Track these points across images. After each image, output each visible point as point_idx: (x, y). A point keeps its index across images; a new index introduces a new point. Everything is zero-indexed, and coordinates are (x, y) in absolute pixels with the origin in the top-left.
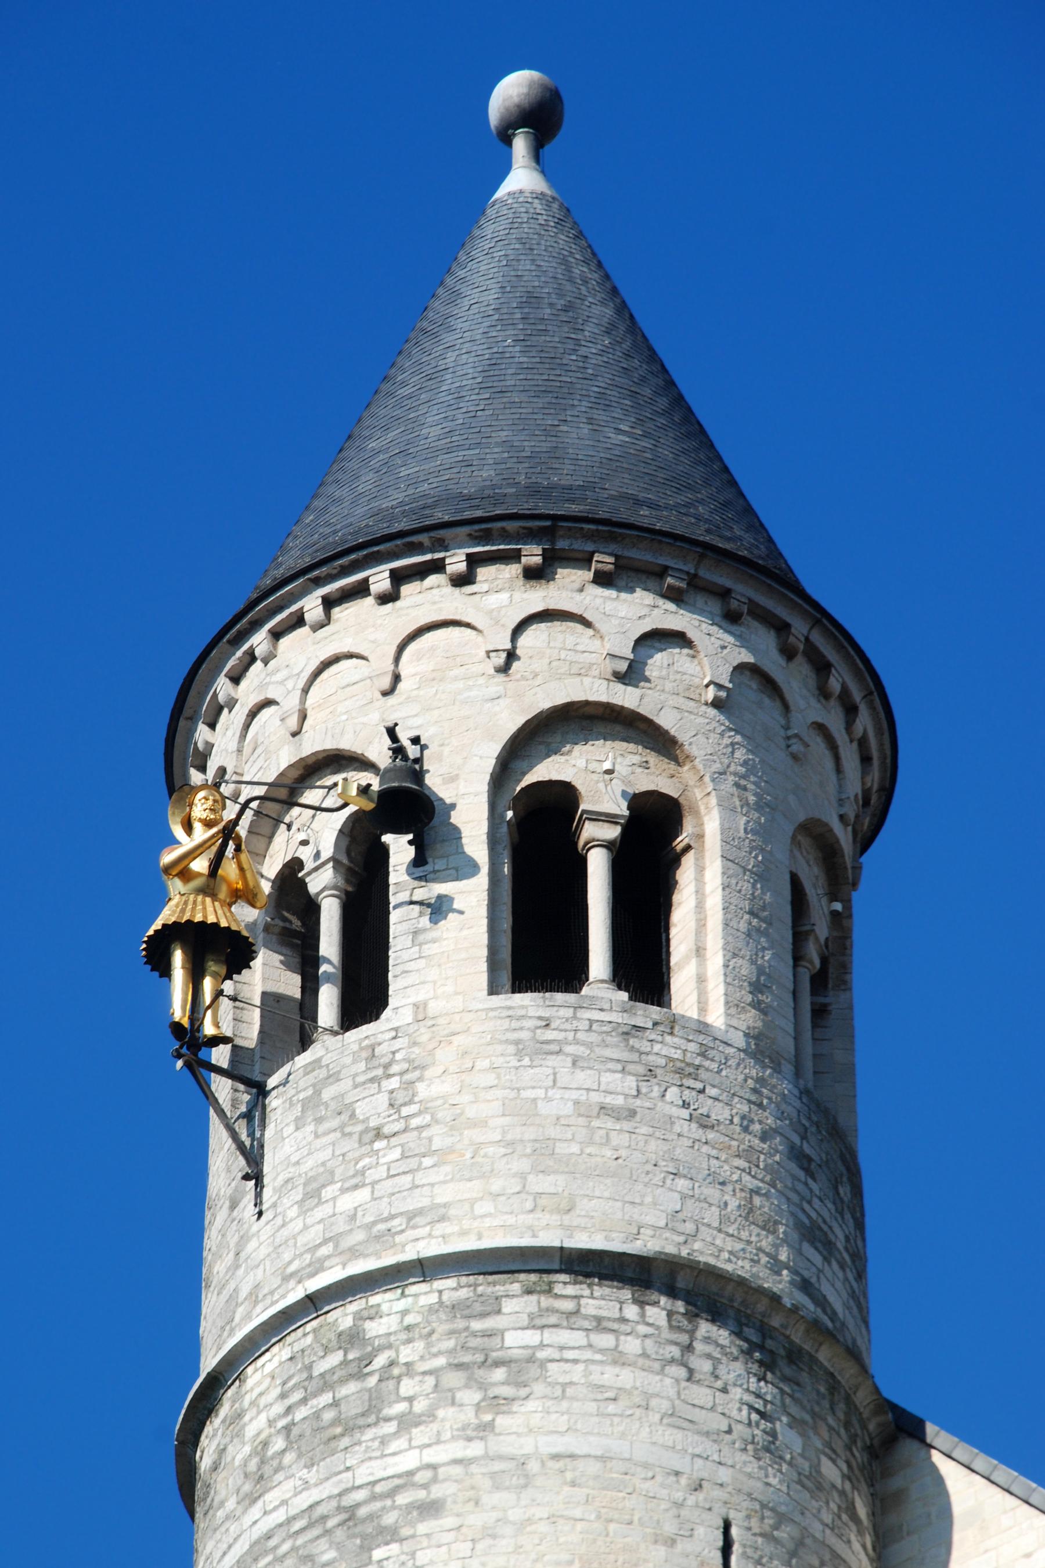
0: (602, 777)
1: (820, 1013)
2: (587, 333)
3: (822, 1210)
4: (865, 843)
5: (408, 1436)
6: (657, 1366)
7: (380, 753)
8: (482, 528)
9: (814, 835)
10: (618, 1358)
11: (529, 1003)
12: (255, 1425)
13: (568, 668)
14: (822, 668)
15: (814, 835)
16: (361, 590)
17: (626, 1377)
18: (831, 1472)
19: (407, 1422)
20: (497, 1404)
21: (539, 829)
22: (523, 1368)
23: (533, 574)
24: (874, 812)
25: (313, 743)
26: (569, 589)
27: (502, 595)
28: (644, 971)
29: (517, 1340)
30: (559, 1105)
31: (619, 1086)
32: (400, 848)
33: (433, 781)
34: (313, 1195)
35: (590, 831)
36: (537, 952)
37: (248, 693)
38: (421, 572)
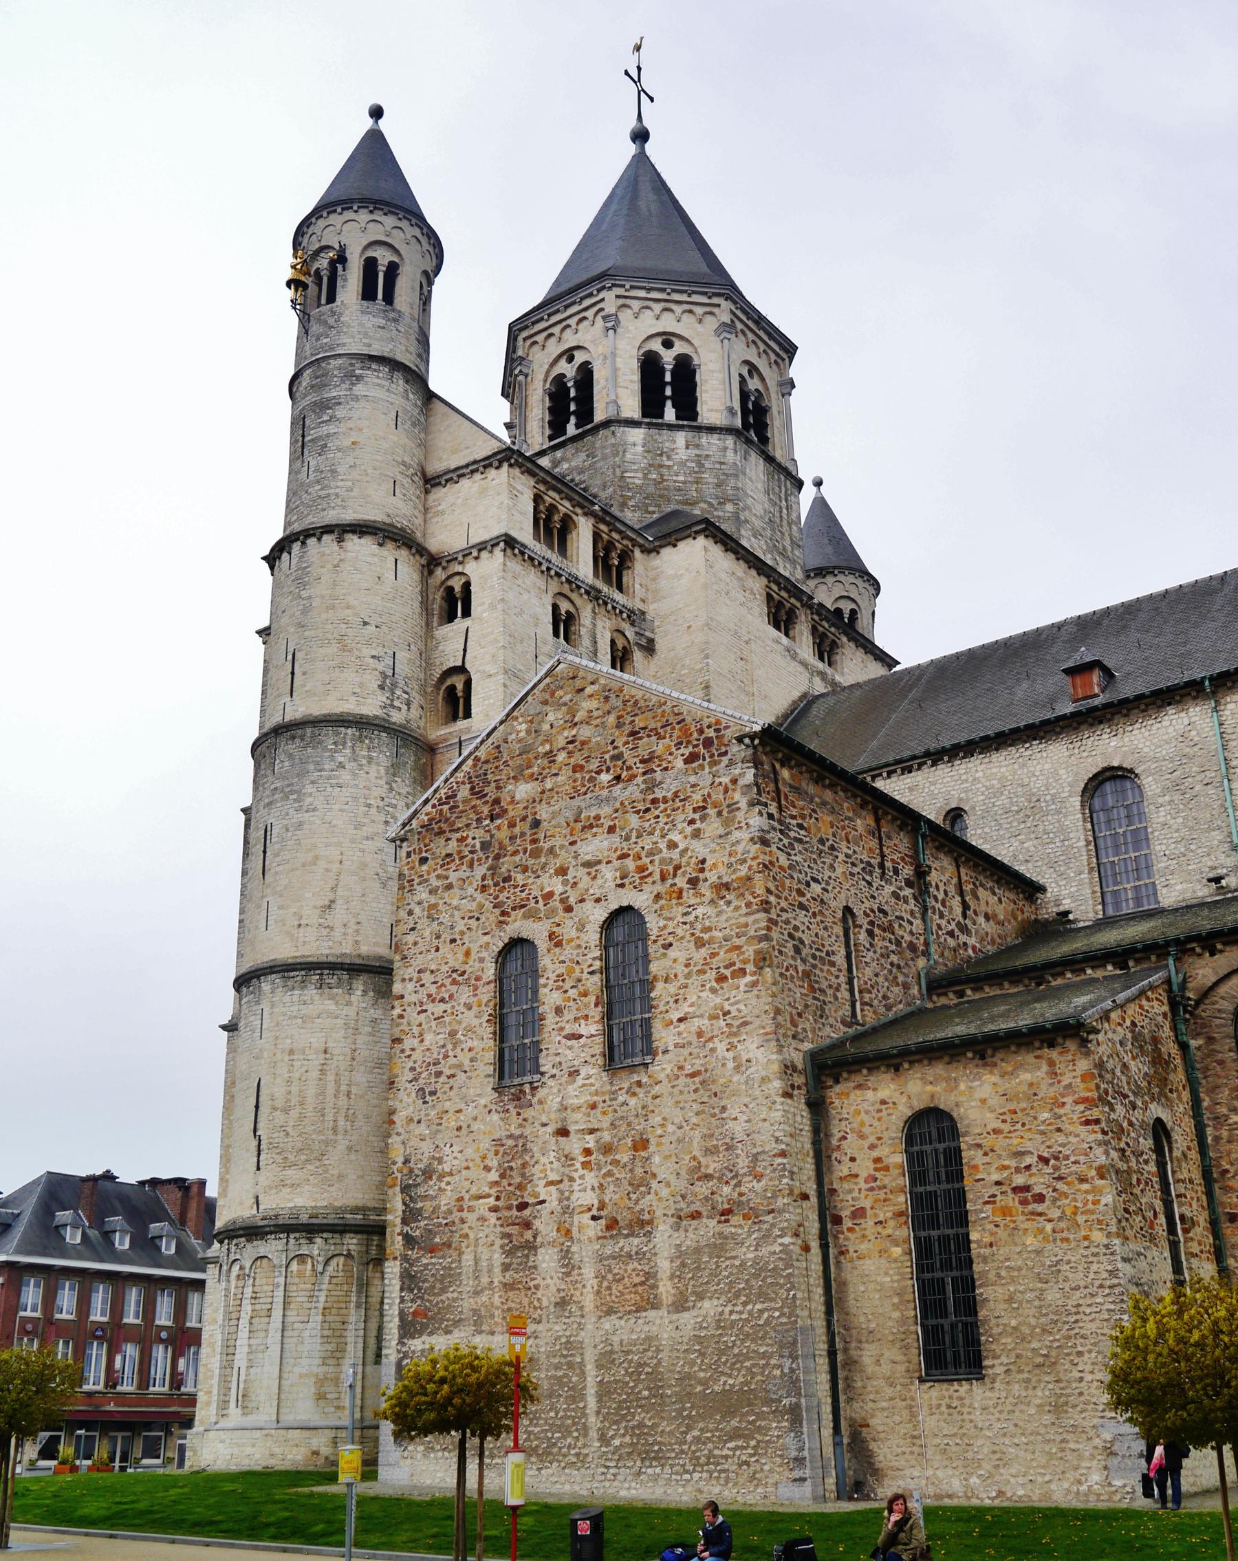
0: (384, 257)
1: (424, 310)
2: (596, 507)
3: (421, 351)
4: (436, 275)
5: (800, 1066)
6: (581, 674)
7: (337, 246)
8: (362, 200)
9: (425, 273)
10: (378, 377)
11: (365, 303)
12: (304, 384)
13: (376, 233)
14: (429, 238)
15: (425, 273)
16: (335, 211)
17: (379, 381)
18: (419, 403)
19: (336, 386)
20: (353, 384)
21: (370, 266)
22: (359, 378)
23: (371, 212)
24: (438, 268)
25: (323, 244)
26: (378, 216)
27: (364, 216)
28: (389, 298)
29: (358, 372)
30: (369, 325)
31: (382, 322)
32: (340, 267)
33: (348, 255)
34: (318, 339)
35: (380, 268)
36: (368, 293)
37: (310, 231)
38: (348, 208)
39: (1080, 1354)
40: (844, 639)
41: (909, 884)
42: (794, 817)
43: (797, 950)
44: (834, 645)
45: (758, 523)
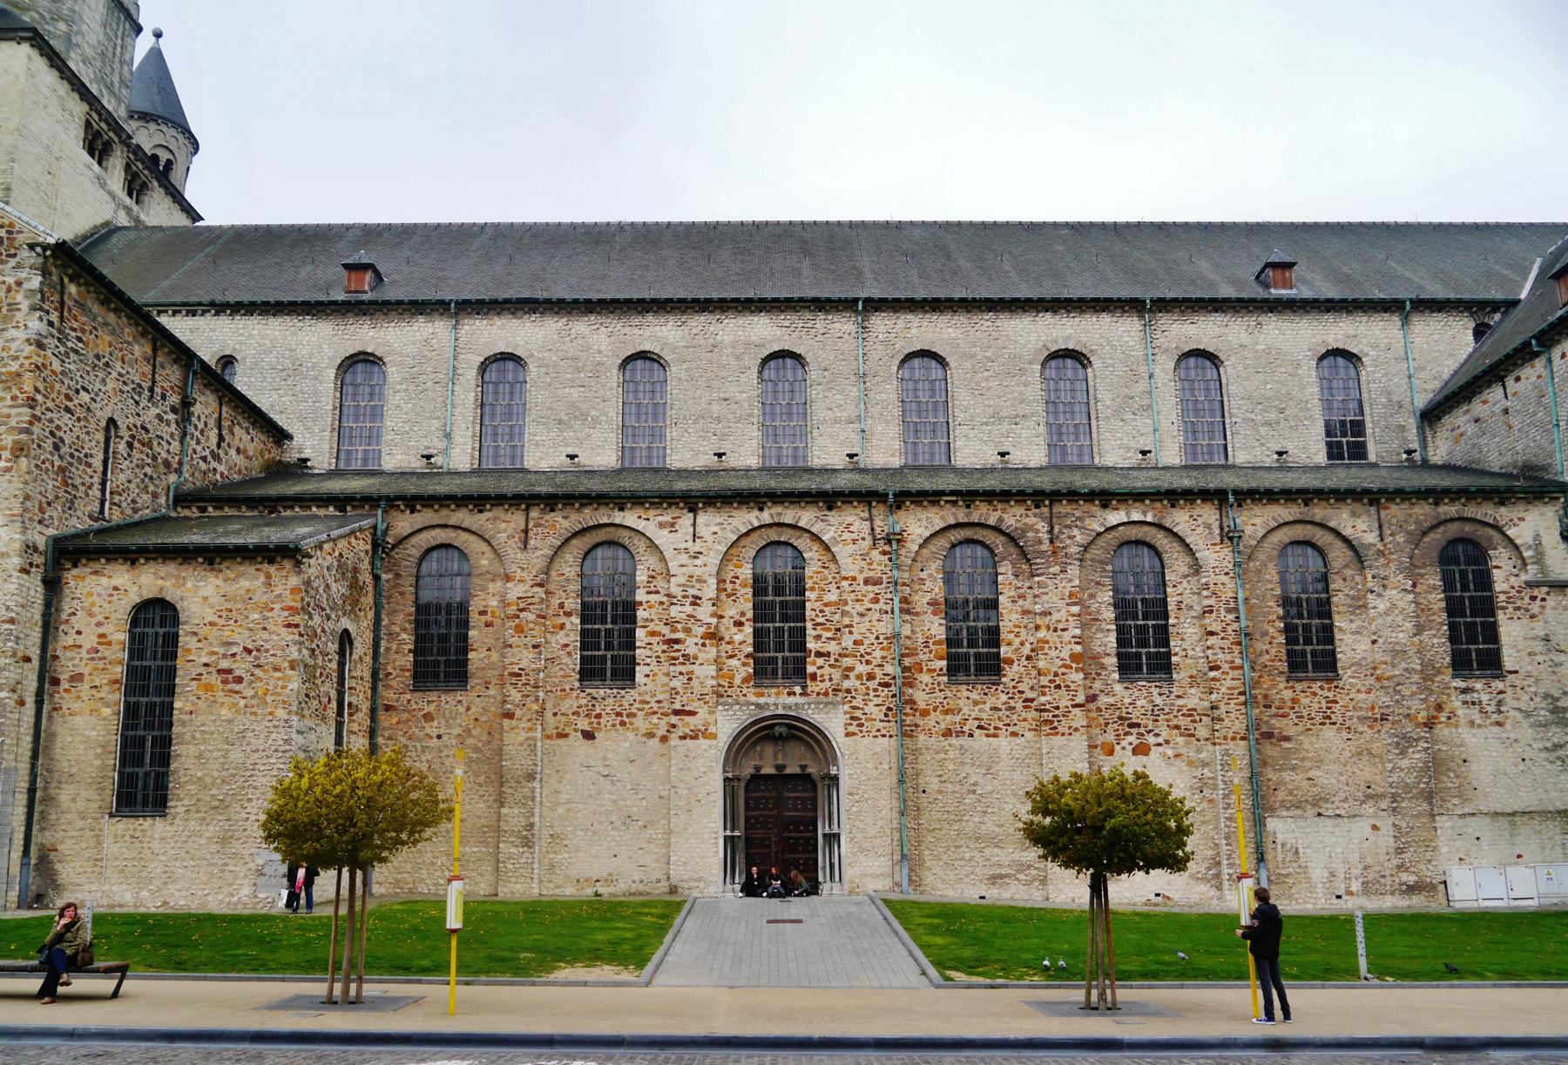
5: (42, 548)
39: (250, 800)
40: (156, 184)
41: (174, 410)
42: (74, 330)
43: (56, 447)
44: (144, 186)
45: (89, 52)
